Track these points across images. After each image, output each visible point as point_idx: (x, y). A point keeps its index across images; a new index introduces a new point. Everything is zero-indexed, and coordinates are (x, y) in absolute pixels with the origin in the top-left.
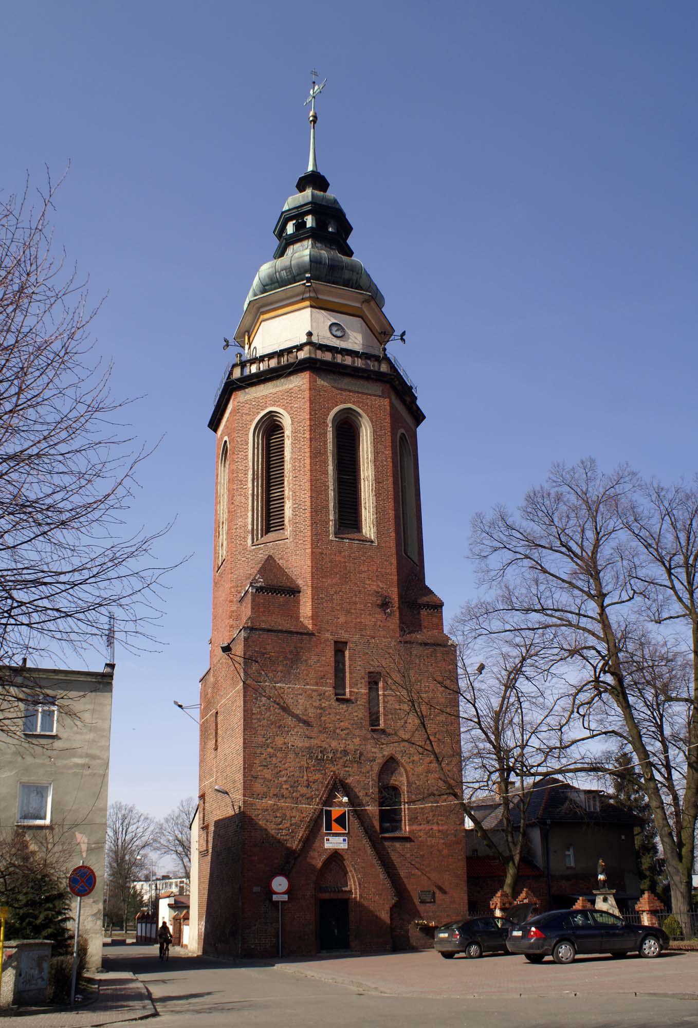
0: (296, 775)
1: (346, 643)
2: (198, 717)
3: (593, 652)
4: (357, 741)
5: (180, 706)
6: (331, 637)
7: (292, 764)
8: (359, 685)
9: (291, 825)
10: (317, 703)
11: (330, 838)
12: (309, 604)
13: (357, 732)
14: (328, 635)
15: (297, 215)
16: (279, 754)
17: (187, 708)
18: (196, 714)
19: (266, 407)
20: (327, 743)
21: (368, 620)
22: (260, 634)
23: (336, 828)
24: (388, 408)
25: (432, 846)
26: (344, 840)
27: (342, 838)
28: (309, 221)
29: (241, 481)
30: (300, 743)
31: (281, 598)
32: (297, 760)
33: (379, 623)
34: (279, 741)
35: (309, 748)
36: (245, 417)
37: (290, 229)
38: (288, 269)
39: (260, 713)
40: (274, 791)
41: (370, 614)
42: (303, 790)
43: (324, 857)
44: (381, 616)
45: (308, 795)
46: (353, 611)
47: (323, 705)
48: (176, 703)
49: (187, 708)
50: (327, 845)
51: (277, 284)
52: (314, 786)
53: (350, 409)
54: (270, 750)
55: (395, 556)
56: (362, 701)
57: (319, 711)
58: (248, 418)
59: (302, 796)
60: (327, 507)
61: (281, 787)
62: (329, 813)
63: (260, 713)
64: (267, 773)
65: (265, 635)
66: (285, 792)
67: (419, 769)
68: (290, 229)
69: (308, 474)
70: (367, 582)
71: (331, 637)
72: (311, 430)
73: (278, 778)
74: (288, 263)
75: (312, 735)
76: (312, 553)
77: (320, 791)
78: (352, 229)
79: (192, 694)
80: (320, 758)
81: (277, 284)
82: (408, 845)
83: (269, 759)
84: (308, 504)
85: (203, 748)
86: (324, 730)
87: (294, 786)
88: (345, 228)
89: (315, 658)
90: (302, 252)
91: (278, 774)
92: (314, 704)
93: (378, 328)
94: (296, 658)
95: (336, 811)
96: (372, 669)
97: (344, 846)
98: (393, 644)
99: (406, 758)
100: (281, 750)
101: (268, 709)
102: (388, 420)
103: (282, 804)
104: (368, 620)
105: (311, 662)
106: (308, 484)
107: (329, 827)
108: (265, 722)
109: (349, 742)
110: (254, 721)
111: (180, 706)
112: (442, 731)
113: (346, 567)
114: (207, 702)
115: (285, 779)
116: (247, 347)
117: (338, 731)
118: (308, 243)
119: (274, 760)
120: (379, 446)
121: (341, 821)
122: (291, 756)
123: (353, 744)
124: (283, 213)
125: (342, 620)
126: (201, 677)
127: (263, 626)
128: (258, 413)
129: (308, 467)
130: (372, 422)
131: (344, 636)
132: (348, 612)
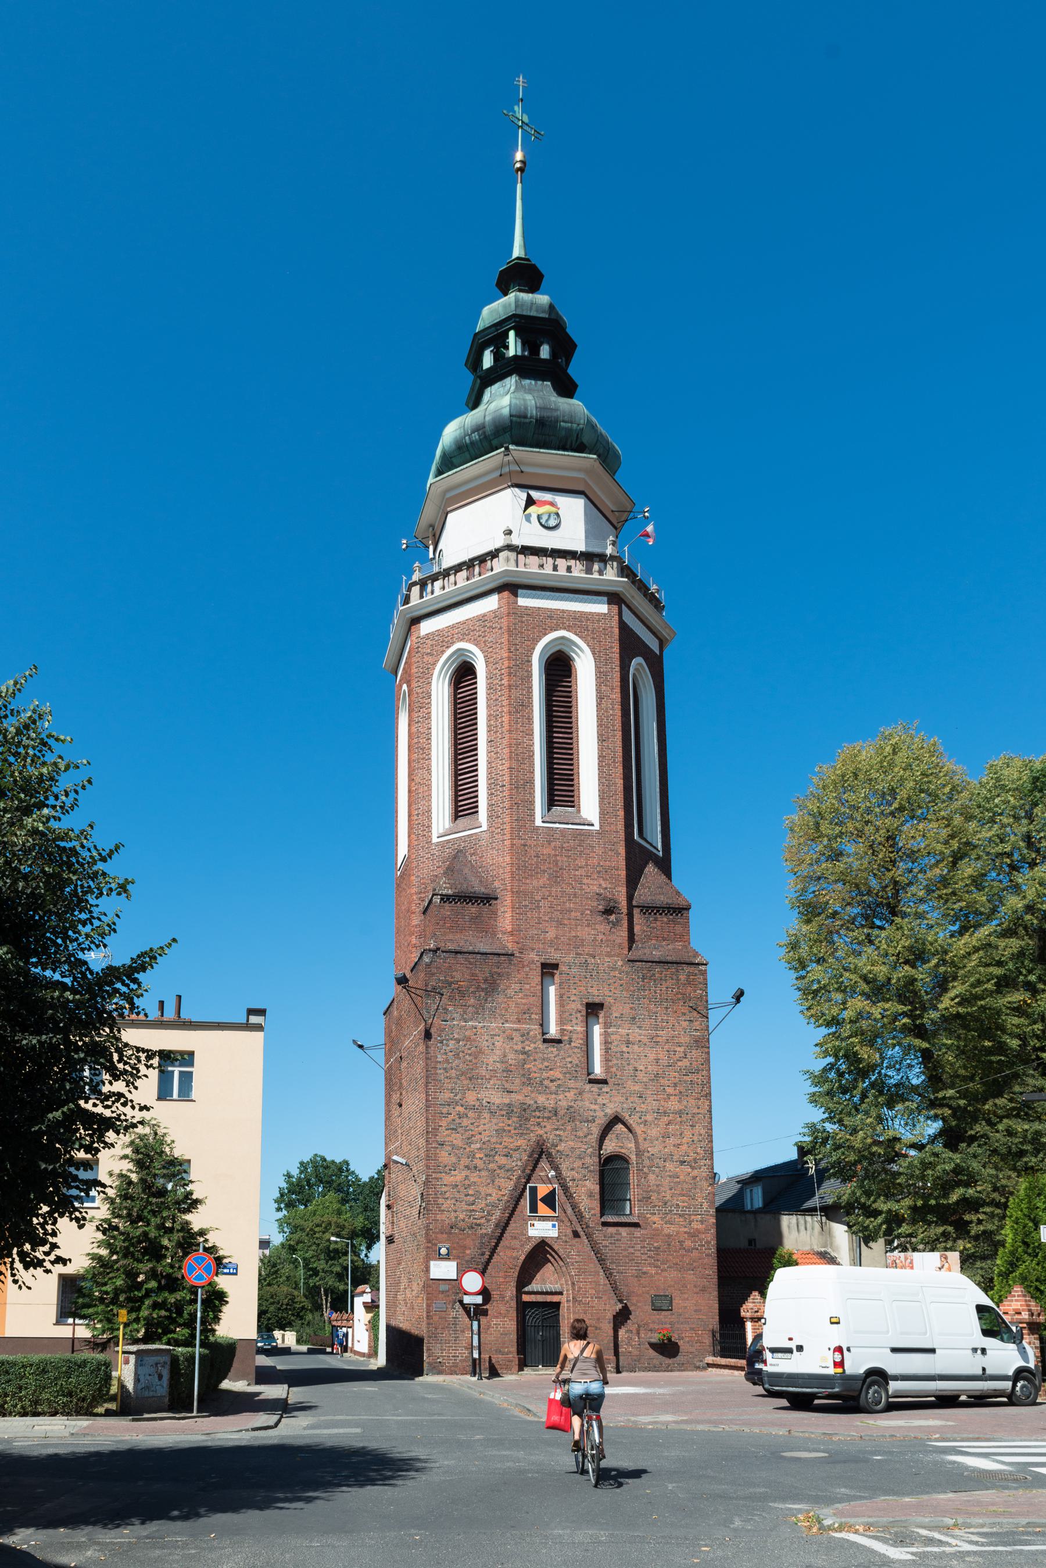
0: (494, 1140)
1: (557, 965)
2: (381, 1060)
3: (272, 1423)
4: (570, 1095)
5: (361, 1047)
6: (537, 958)
7: (488, 1127)
8: (574, 1021)
9: (487, 1205)
10: (519, 1047)
11: (536, 1223)
12: (508, 915)
13: (571, 1084)
14: (533, 956)
15: (495, 337)
16: (471, 1114)
17: (369, 1048)
18: (380, 1055)
19: (453, 643)
20: (532, 1099)
21: (585, 933)
22: (446, 958)
23: (543, 1209)
24: (616, 631)
25: (669, 1236)
26: (554, 1226)
27: (550, 1224)
28: (513, 346)
29: (423, 749)
30: (498, 1099)
31: (473, 909)
32: (494, 1121)
33: (601, 937)
34: (471, 1097)
35: (509, 1105)
36: (426, 658)
37: (488, 360)
38: (479, 428)
39: (447, 1061)
40: (465, 1161)
41: (588, 925)
42: (502, 1160)
43: (528, 1248)
44: (603, 927)
45: (507, 1167)
46: (566, 922)
47: (527, 1048)
48: (354, 1042)
49: (369, 1048)
50: (532, 1232)
51: (467, 455)
52: (516, 1155)
53: (563, 638)
54: (459, 1108)
55: (623, 843)
56: (578, 1042)
57: (521, 1057)
58: (430, 659)
59: (500, 1168)
60: (531, 782)
61: (474, 1157)
62: (534, 1190)
63: (447, 1061)
64: (457, 1139)
65: (451, 959)
66: (480, 1164)
67: (654, 1132)
68: (488, 360)
69: (507, 736)
70: (585, 881)
71: (537, 958)
72: (510, 674)
73: (469, 1144)
74: (480, 420)
75: (513, 1088)
76: (512, 845)
77: (518, 1161)
78: (575, 346)
79: (375, 1033)
80: (524, 1114)
81: (467, 455)
82: (637, 1232)
83: (458, 1121)
84: (507, 778)
85: (388, 1103)
86: (528, 1081)
87: (490, 1156)
88: (565, 347)
89: (517, 987)
90: (502, 399)
91: (469, 1141)
92: (515, 1047)
93: (609, 505)
94: (491, 986)
95: (543, 1190)
96: (590, 1000)
97: (554, 1233)
98: (620, 963)
99: (636, 1117)
100: (473, 1108)
101: (457, 1056)
102: (616, 649)
103: (474, 1177)
104: (585, 933)
105: (510, 992)
106: (506, 751)
107: (534, 1209)
108: (453, 1073)
109: (561, 1097)
110: (439, 1072)
111: (361, 1047)
112: (685, 1082)
113: (556, 862)
114: (392, 1043)
115: (478, 1146)
116: (431, 548)
117: (546, 1082)
118: (511, 381)
119: (465, 1122)
120: (604, 688)
121: (550, 1200)
122: (486, 1115)
123: (565, 1100)
124: (476, 335)
125: (551, 934)
126: (385, 1008)
127: (451, 947)
128: (443, 652)
129: (506, 727)
130: (594, 654)
131: (554, 956)
132: (560, 923)
